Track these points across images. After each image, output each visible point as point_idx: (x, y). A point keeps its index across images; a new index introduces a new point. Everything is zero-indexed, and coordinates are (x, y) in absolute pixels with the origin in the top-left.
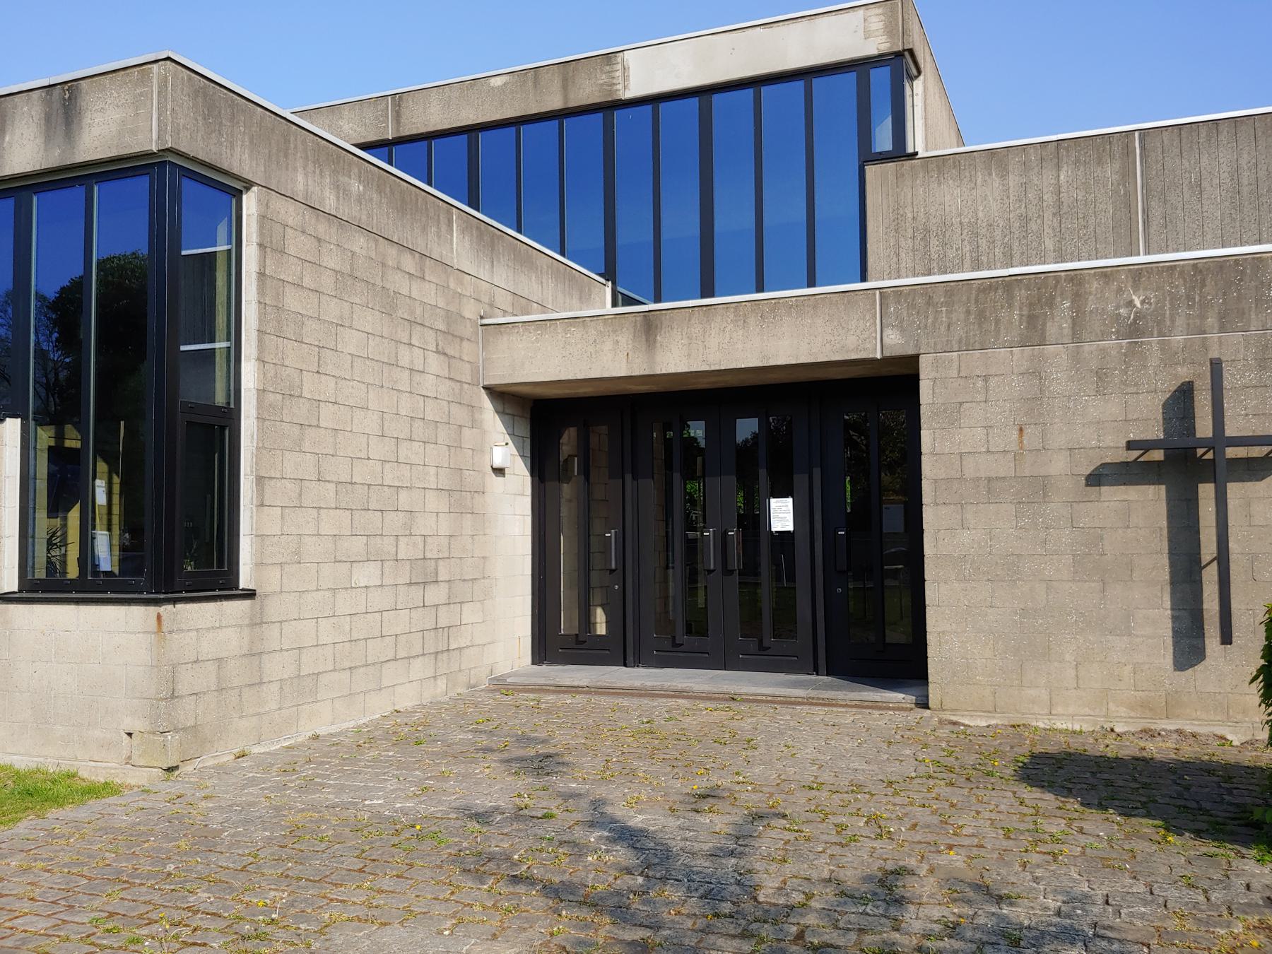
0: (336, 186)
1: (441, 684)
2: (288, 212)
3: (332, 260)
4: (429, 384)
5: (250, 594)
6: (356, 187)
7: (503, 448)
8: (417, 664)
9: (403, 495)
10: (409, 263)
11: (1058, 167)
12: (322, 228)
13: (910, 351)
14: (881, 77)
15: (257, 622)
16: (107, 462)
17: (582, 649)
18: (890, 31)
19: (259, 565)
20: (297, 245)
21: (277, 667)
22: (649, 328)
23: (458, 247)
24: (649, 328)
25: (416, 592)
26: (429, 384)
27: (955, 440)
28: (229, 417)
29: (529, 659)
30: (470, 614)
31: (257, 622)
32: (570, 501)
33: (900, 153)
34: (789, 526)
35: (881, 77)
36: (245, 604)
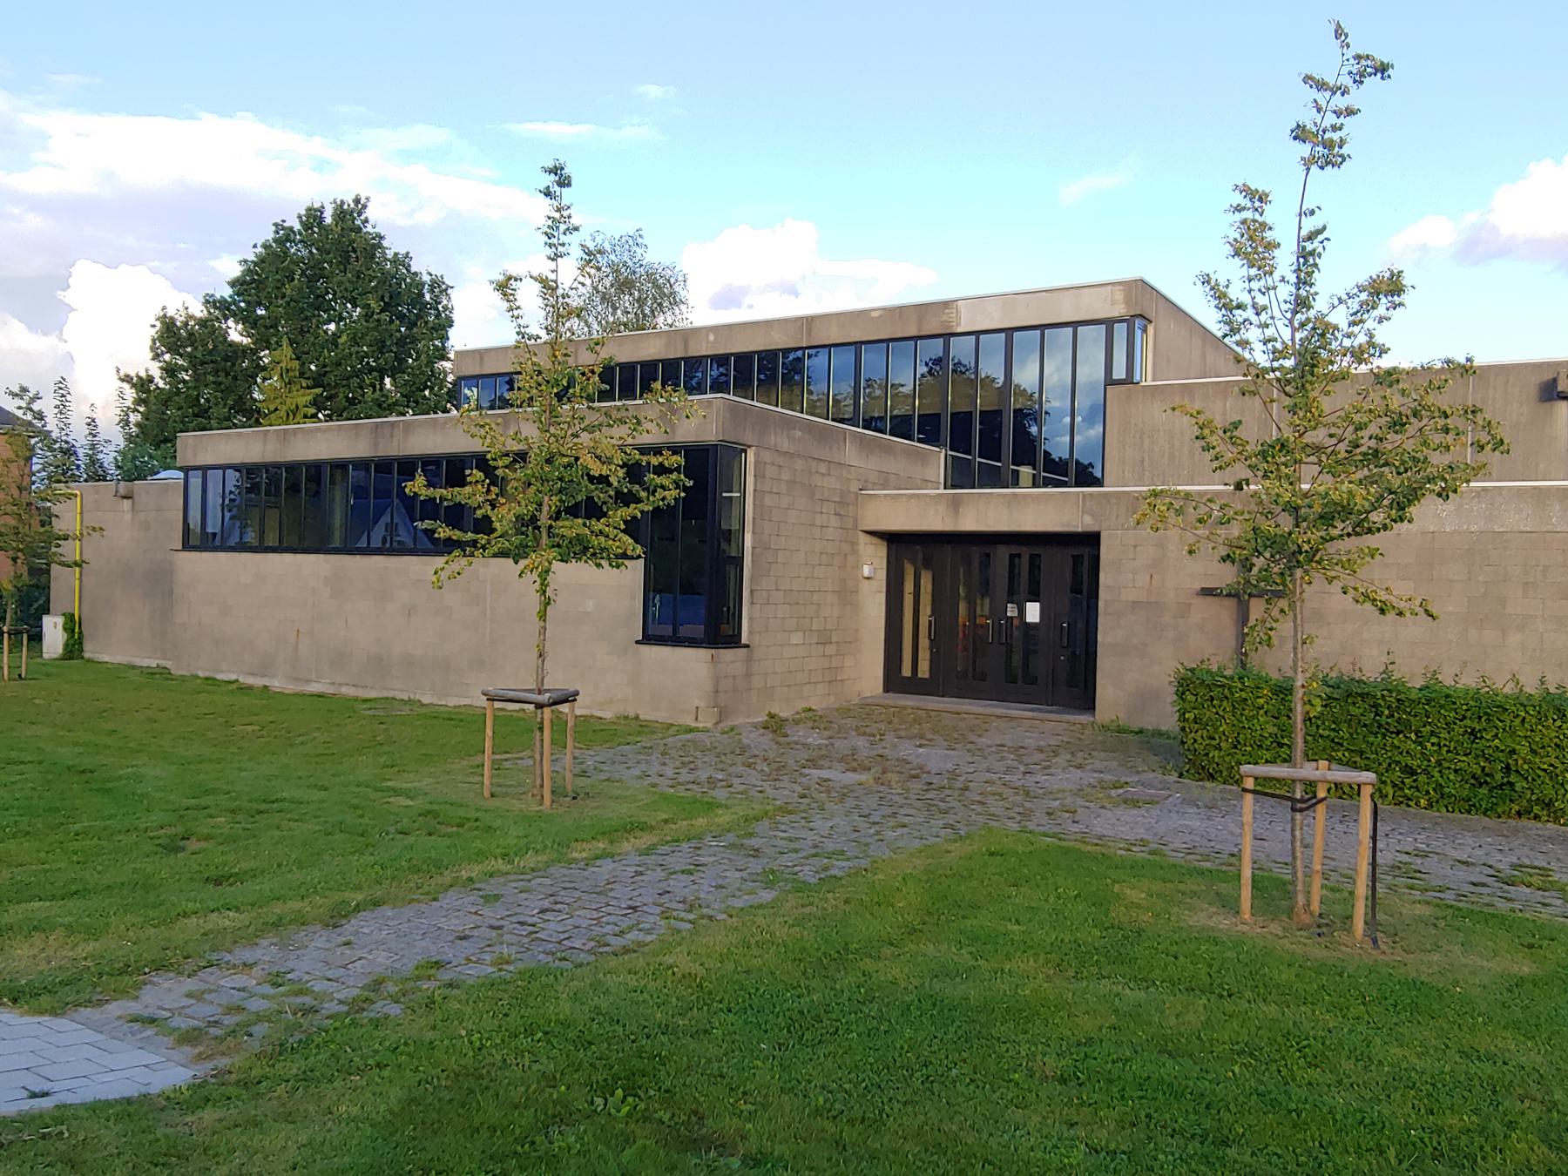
0: (788, 437)
1: (832, 699)
2: (767, 456)
3: (786, 476)
4: (830, 533)
5: (747, 646)
6: (798, 434)
7: (872, 563)
8: (820, 686)
9: (816, 596)
10: (823, 468)
11: (1226, 398)
12: (781, 461)
13: (1095, 529)
14: (1120, 331)
15: (749, 660)
16: (232, 344)
17: (913, 686)
18: (1127, 302)
19: (750, 633)
20: (770, 472)
21: (757, 682)
22: (956, 503)
23: (850, 454)
24: (956, 503)
25: (821, 647)
26: (830, 533)
27: (1118, 581)
28: (739, 561)
29: (880, 689)
30: (848, 661)
31: (749, 660)
32: (612, 842)
33: (1129, 380)
34: (1037, 620)
35: (1120, 331)
36: (744, 650)
